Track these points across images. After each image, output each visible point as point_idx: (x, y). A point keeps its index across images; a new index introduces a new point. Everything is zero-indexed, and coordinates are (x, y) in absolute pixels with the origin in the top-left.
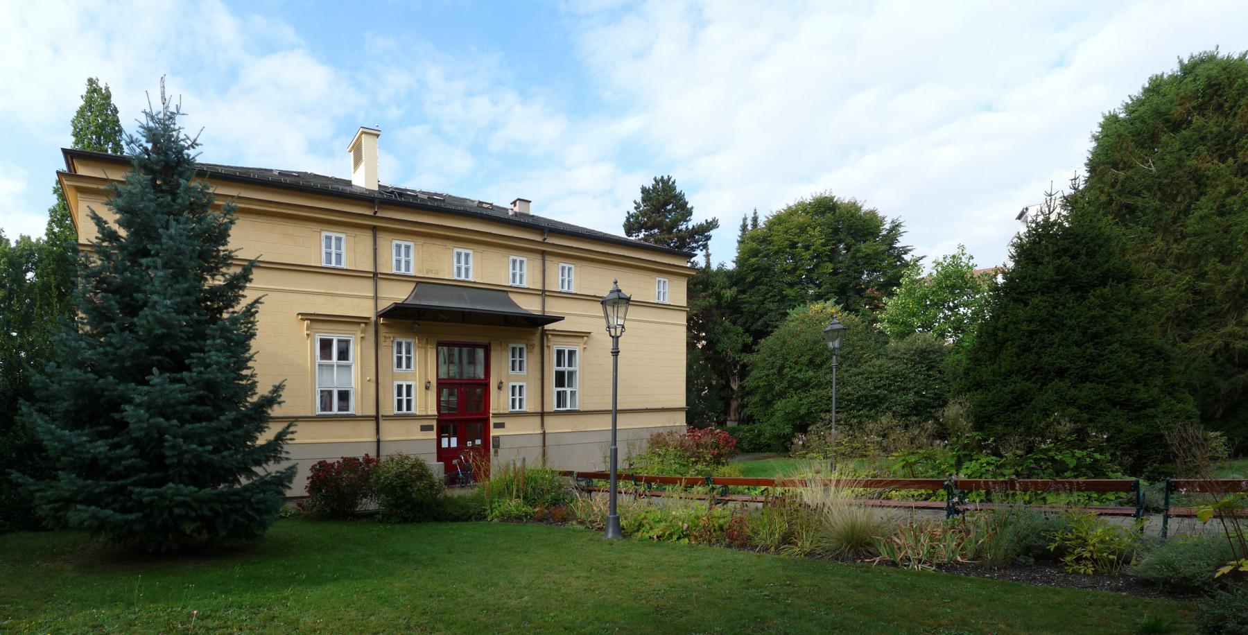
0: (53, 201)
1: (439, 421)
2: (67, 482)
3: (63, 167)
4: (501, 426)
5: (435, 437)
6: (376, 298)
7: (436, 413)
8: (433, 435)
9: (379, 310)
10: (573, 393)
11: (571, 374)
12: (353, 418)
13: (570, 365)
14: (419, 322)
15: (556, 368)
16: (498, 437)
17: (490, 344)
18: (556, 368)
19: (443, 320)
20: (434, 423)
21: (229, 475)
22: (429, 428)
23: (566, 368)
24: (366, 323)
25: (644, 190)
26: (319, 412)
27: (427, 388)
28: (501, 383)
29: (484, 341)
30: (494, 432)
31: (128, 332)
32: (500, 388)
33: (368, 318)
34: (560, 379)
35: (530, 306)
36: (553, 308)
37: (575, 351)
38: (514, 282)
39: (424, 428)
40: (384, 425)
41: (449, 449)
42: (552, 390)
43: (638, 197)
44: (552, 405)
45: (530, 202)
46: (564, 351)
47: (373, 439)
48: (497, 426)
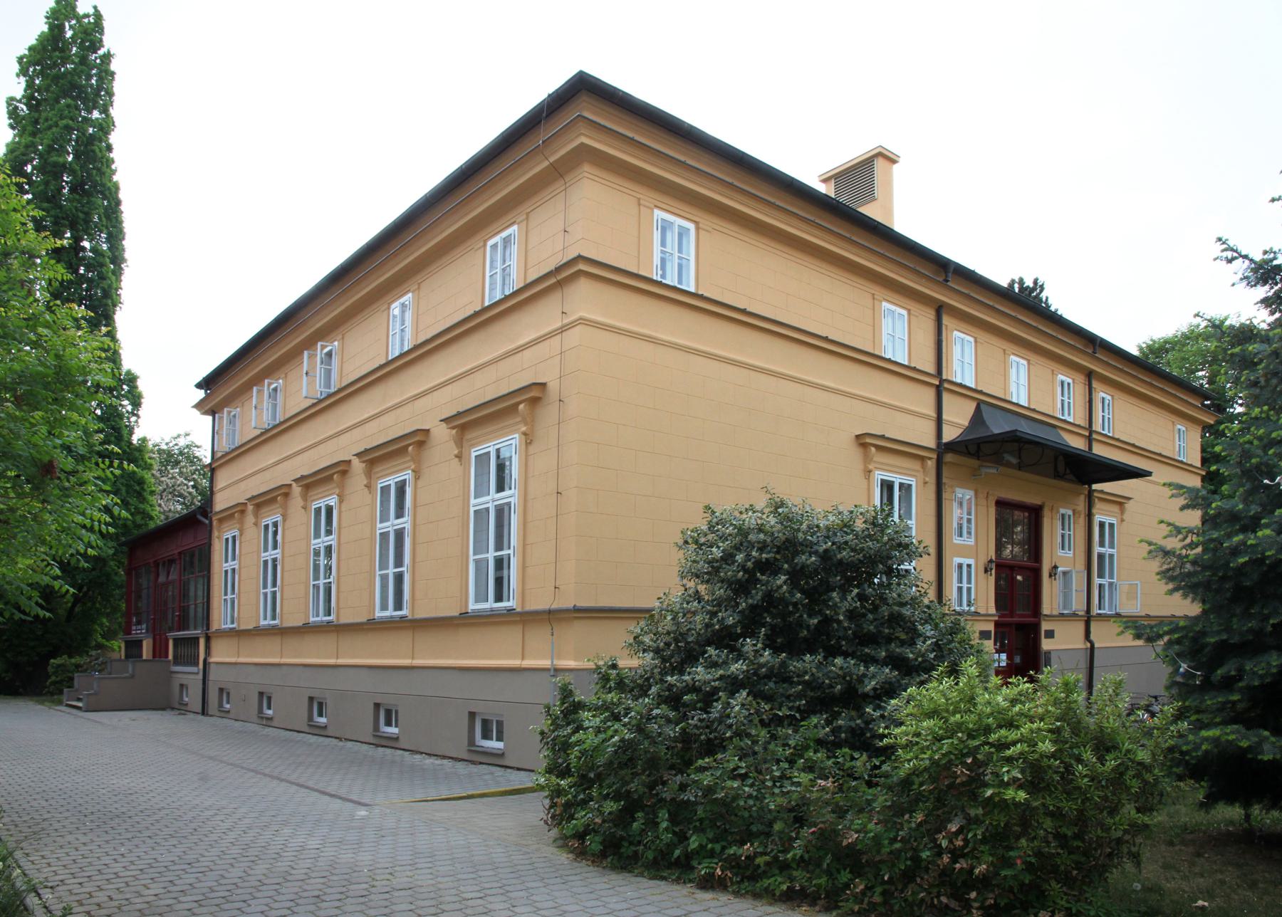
29: (1032, 499)
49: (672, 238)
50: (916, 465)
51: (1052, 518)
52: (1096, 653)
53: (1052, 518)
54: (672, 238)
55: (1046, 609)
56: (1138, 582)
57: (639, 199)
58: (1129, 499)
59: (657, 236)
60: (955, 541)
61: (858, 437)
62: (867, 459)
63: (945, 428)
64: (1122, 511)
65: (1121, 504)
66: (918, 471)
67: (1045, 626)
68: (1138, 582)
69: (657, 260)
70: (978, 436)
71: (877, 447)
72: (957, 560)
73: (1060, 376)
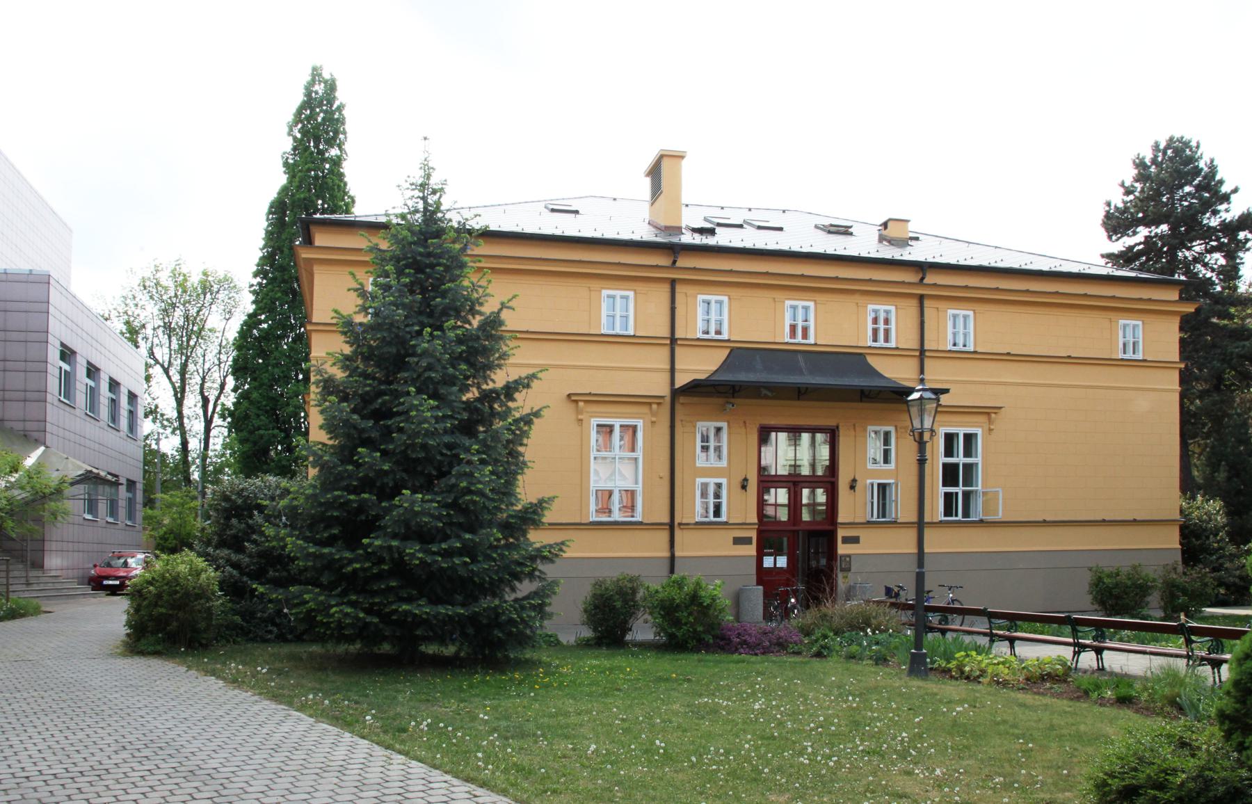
0: (309, 78)
1: (760, 532)
2: (271, 426)
3: (326, 76)
4: (855, 540)
5: (755, 553)
6: (672, 370)
7: (756, 521)
8: (751, 550)
9: (677, 386)
10: (967, 495)
11: (969, 468)
12: (894, 523)
13: (968, 453)
14: (732, 400)
15: (943, 459)
16: (849, 556)
17: (838, 427)
18: (943, 459)
19: (766, 397)
20: (753, 534)
21: (493, 589)
22: (747, 541)
23: (960, 459)
24: (659, 404)
25: (1140, 164)
26: (594, 518)
27: (744, 487)
28: (854, 480)
29: (831, 423)
30: (842, 549)
31: (415, 377)
32: (852, 487)
33: (662, 397)
34: (950, 475)
35: (898, 372)
36: (937, 374)
37: (976, 434)
38: (875, 340)
39: (738, 541)
40: (928, 534)
41: (775, 570)
42: (937, 490)
43: (1129, 175)
44: (936, 509)
45: (907, 221)
46: (957, 434)
47: (667, 554)
48: (847, 540)
49: (960, 322)
50: (645, 409)
51: (855, 436)
52: (676, 560)
53: (855, 436)
54: (960, 322)
55: (840, 520)
56: (1000, 490)
57: (686, 294)
58: (1000, 408)
59: (950, 324)
60: (869, 467)
61: (569, 396)
62: (578, 412)
63: (677, 375)
64: (990, 421)
65: (988, 414)
66: (646, 414)
67: (841, 533)
68: (1000, 490)
69: (950, 337)
70: (847, 384)
71: (586, 401)
72: (699, 481)
73: (949, 311)
